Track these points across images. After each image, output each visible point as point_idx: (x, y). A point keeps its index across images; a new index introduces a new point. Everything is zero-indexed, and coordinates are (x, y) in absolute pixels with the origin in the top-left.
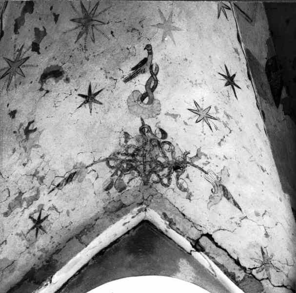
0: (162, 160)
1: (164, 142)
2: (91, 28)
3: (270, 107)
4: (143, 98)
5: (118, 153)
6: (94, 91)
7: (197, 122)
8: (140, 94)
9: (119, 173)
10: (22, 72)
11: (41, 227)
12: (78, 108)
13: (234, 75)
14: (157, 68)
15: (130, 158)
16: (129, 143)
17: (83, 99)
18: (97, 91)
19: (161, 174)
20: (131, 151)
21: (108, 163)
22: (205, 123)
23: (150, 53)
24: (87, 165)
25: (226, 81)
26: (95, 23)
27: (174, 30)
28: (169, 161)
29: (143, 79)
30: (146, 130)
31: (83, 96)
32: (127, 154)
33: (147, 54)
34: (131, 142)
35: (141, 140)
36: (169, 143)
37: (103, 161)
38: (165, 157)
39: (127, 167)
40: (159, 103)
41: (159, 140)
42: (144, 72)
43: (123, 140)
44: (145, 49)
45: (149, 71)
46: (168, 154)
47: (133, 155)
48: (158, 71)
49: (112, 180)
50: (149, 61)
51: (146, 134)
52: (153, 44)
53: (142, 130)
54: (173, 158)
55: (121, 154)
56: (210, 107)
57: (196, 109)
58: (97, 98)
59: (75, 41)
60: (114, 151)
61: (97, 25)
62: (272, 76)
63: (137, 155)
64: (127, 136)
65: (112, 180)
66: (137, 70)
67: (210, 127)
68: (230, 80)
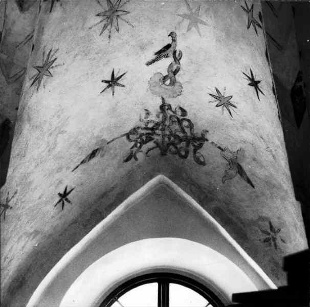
0: (181, 135)
1: (184, 119)
2: (116, 18)
3: (271, 174)
4: (165, 78)
5: (138, 128)
6: (116, 76)
7: (217, 106)
8: (162, 76)
9: (139, 145)
10: (50, 74)
11: (67, 200)
12: (101, 93)
13: (259, 82)
14: (181, 54)
15: (150, 132)
16: (150, 118)
17: (106, 85)
18: (119, 75)
19: (179, 146)
20: (150, 125)
21: (128, 138)
22: (225, 108)
24: (109, 141)
25: (250, 82)
26: (119, 13)
27: (200, 23)
28: (187, 136)
29: (164, 64)
30: (166, 107)
31: (106, 82)
32: (146, 128)
33: (171, 41)
34: (150, 118)
35: (161, 116)
36: (189, 121)
37: (123, 136)
38: (184, 132)
39: (146, 139)
40: (181, 86)
41: (179, 117)
42: (167, 57)
43: (143, 115)
44: (169, 36)
45: (172, 56)
46: (187, 130)
47: (152, 129)
48: (182, 55)
49: (132, 151)
50: (173, 46)
51: (167, 111)
52: (178, 33)
53: (162, 108)
54: (191, 134)
55: (141, 128)
56: (232, 97)
57: (217, 95)
58: (119, 82)
59: (99, 33)
60: (135, 126)
61: (122, 15)
62: (297, 100)
63: (157, 129)
64: (148, 113)
65: (132, 151)
66: (160, 54)
67: (230, 113)
68: (254, 83)
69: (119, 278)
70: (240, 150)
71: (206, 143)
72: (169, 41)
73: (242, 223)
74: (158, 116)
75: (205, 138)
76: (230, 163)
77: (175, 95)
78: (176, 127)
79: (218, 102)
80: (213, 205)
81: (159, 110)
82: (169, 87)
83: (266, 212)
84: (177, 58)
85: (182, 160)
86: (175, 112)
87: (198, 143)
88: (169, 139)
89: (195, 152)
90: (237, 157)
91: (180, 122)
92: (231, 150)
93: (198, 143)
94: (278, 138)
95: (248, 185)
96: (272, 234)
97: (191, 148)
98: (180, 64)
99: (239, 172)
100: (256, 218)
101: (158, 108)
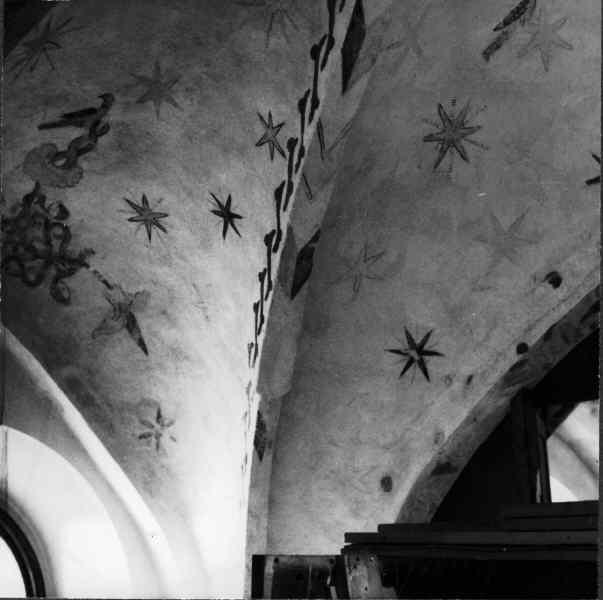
0: (39, 246)
19: (28, 264)
23: (106, 106)
36: (66, 229)
38: (48, 243)
40: (81, 174)
46: (56, 244)
50: (99, 113)
53: (28, 198)
57: (141, 205)
69: (246, 580)
70: (146, 294)
71: (84, 269)
72: (98, 103)
73: (109, 405)
74: (13, 209)
75: (86, 261)
76: (115, 309)
77: (62, 185)
78: (39, 233)
79: (135, 215)
80: (66, 372)
81: (21, 201)
82: (60, 172)
83: (157, 394)
84: (97, 131)
85: (25, 288)
86: (47, 211)
87: (68, 267)
88: (15, 249)
89: (56, 280)
90: (132, 302)
91: (48, 226)
92: (125, 290)
93: (68, 267)
94: (555, 457)
95: (139, 349)
96: (157, 426)
97: (53, 272)
98: (96, 141)
99: (128, 326)
100: (138, 400)
101: (21, 197)
